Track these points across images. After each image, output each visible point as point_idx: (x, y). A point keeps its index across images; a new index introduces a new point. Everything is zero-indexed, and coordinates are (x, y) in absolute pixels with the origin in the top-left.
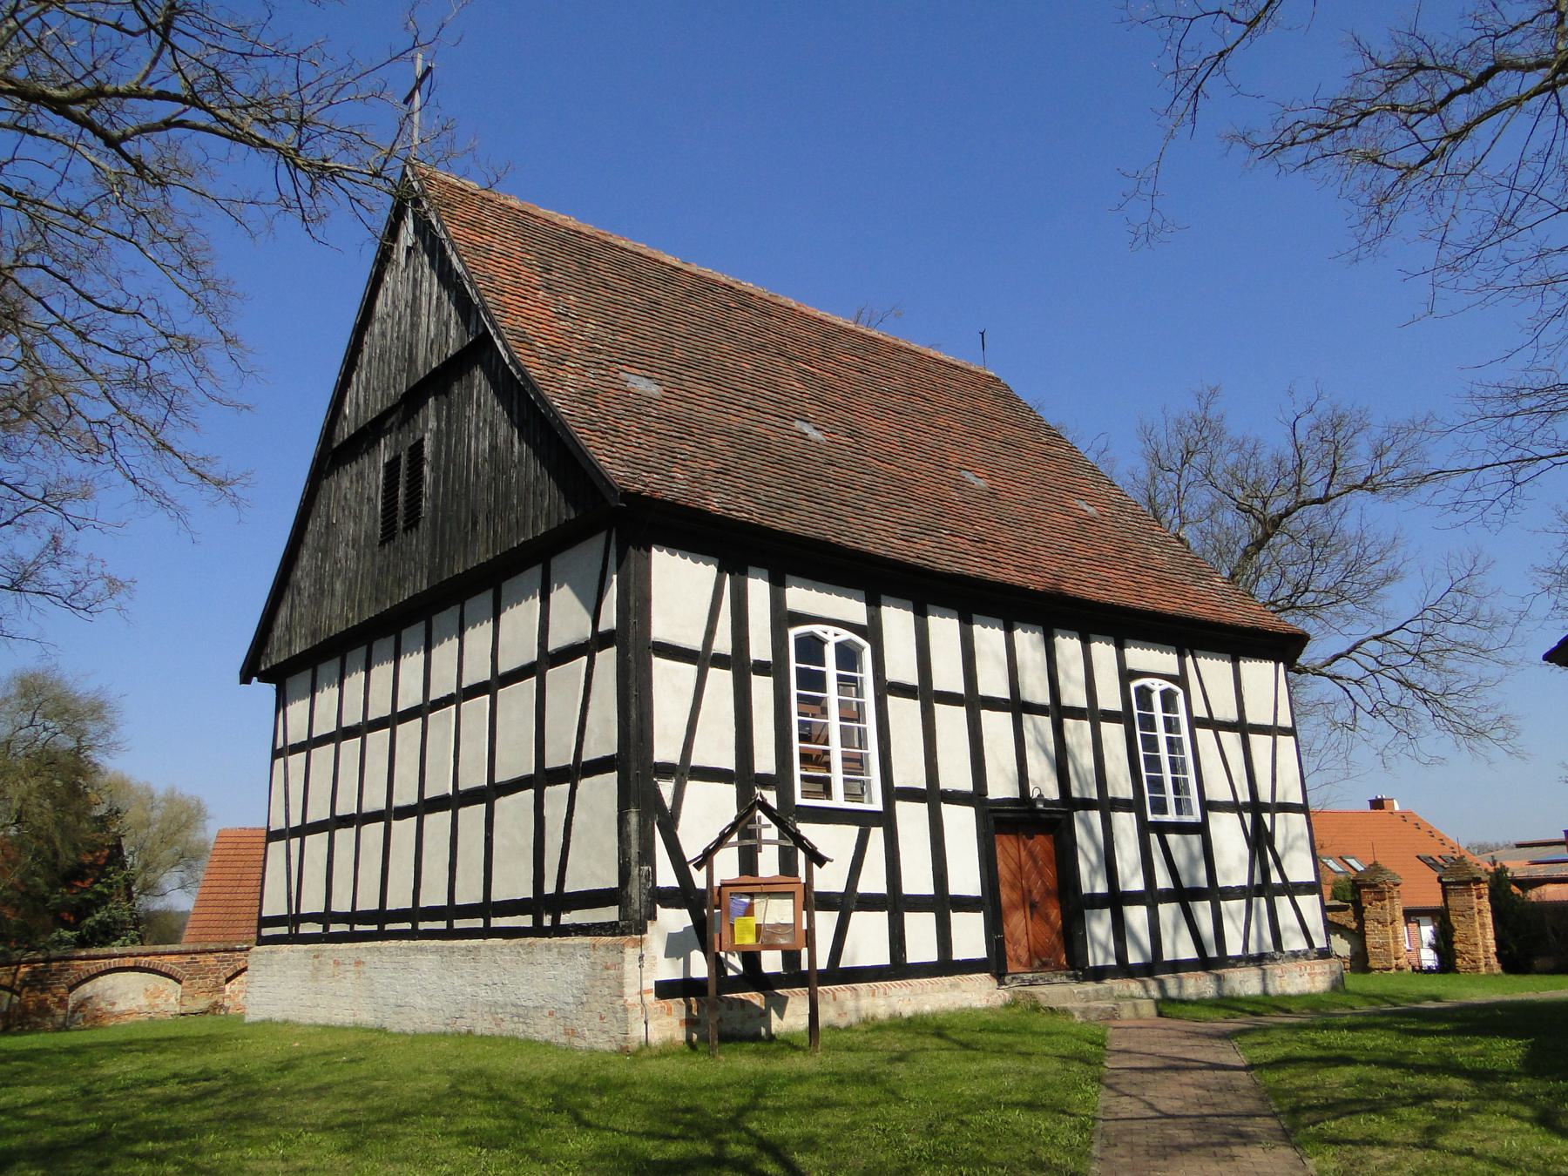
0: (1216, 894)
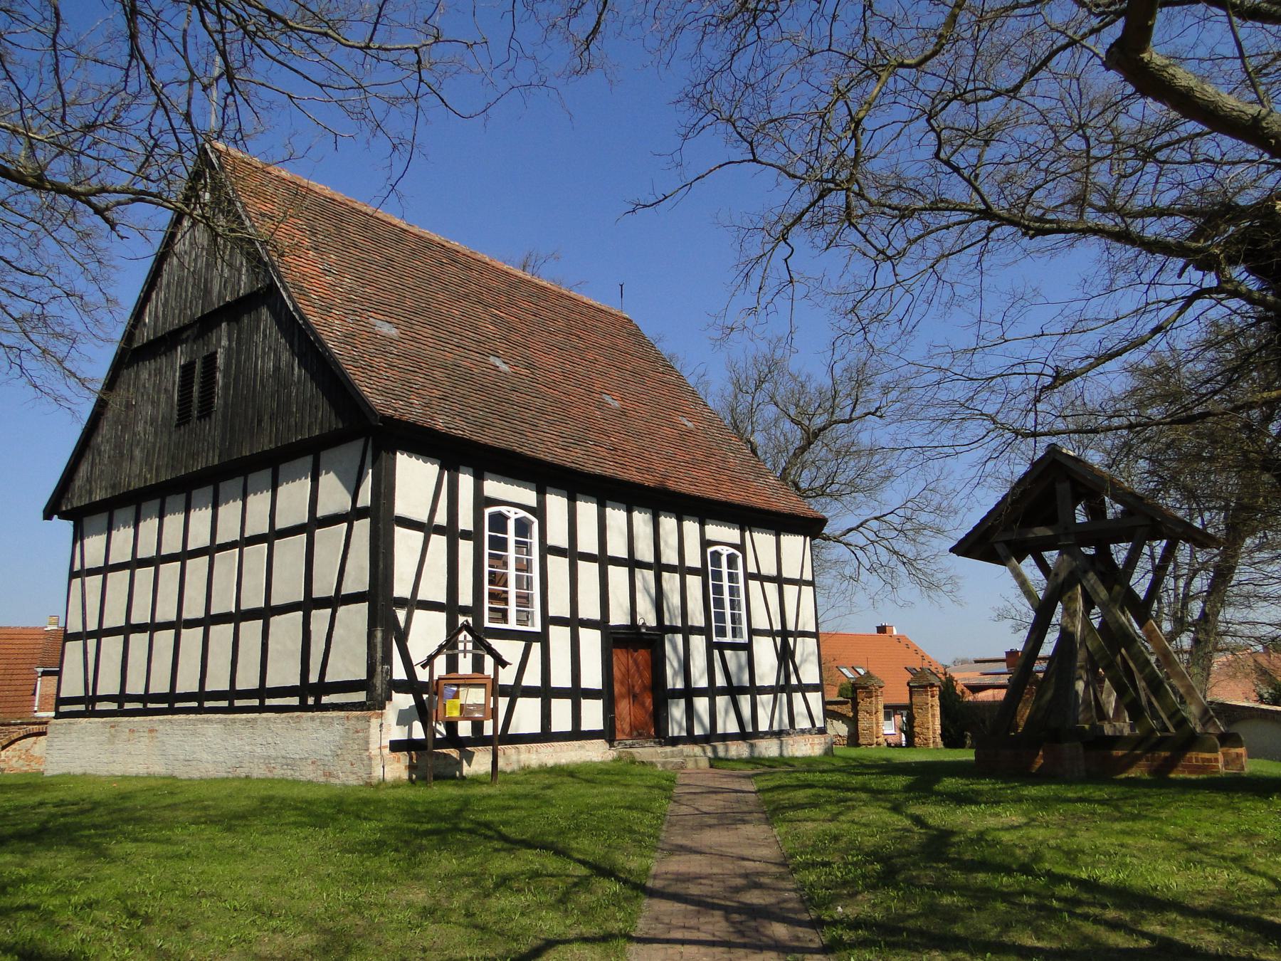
0: (754, 690)
